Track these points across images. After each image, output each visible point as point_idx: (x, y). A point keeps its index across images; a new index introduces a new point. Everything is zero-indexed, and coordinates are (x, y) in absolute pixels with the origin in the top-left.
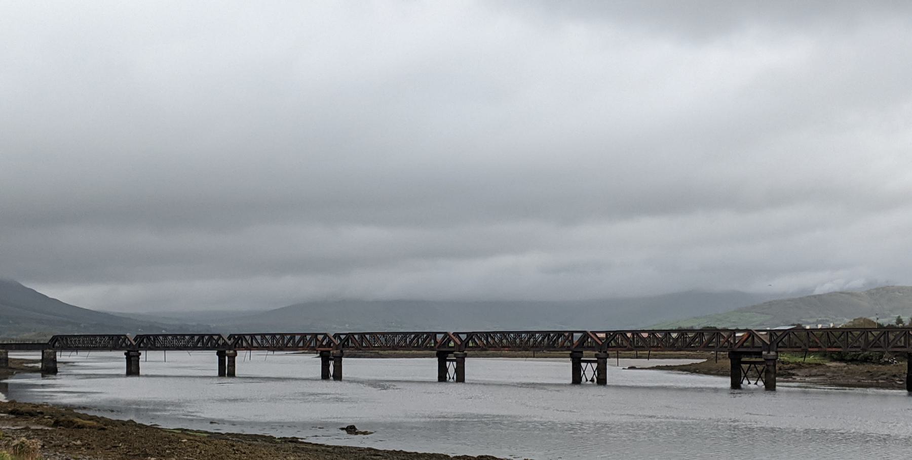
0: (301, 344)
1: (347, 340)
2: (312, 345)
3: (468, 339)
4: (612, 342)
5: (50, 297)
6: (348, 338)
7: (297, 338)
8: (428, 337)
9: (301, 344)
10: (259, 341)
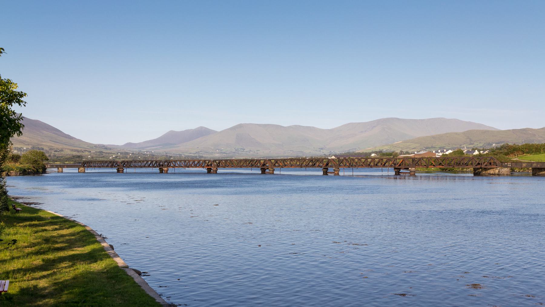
0: (372, 164)
1: (219, 163)
2: (203, 165)
3: (275, 163)
4: (341, 164)
5: (285, 126)
6: (219, 162)
7: (196, 162)
8: (257, 161)
9: (198, 165)
10: (179, 163)
